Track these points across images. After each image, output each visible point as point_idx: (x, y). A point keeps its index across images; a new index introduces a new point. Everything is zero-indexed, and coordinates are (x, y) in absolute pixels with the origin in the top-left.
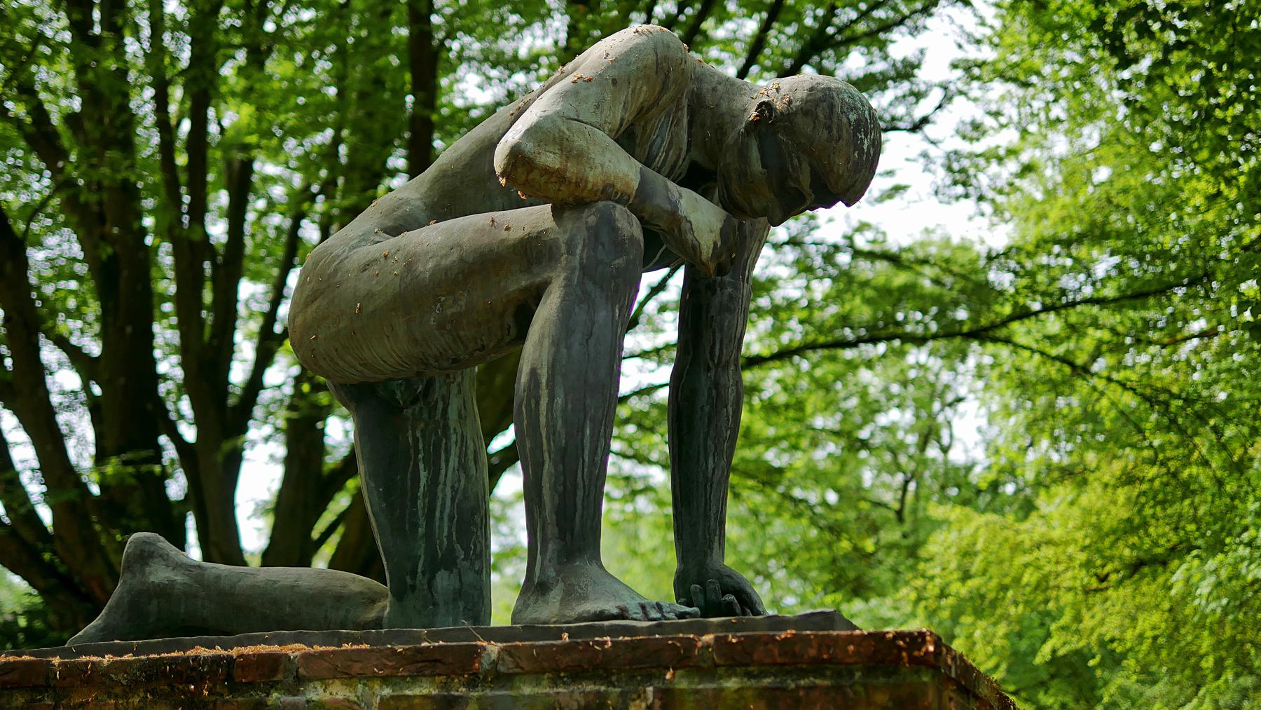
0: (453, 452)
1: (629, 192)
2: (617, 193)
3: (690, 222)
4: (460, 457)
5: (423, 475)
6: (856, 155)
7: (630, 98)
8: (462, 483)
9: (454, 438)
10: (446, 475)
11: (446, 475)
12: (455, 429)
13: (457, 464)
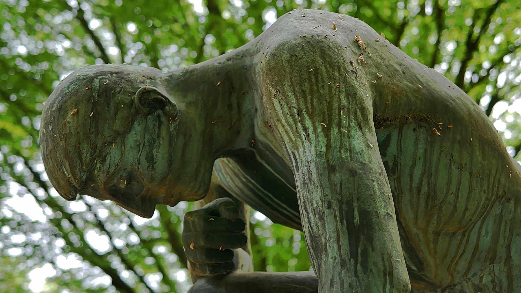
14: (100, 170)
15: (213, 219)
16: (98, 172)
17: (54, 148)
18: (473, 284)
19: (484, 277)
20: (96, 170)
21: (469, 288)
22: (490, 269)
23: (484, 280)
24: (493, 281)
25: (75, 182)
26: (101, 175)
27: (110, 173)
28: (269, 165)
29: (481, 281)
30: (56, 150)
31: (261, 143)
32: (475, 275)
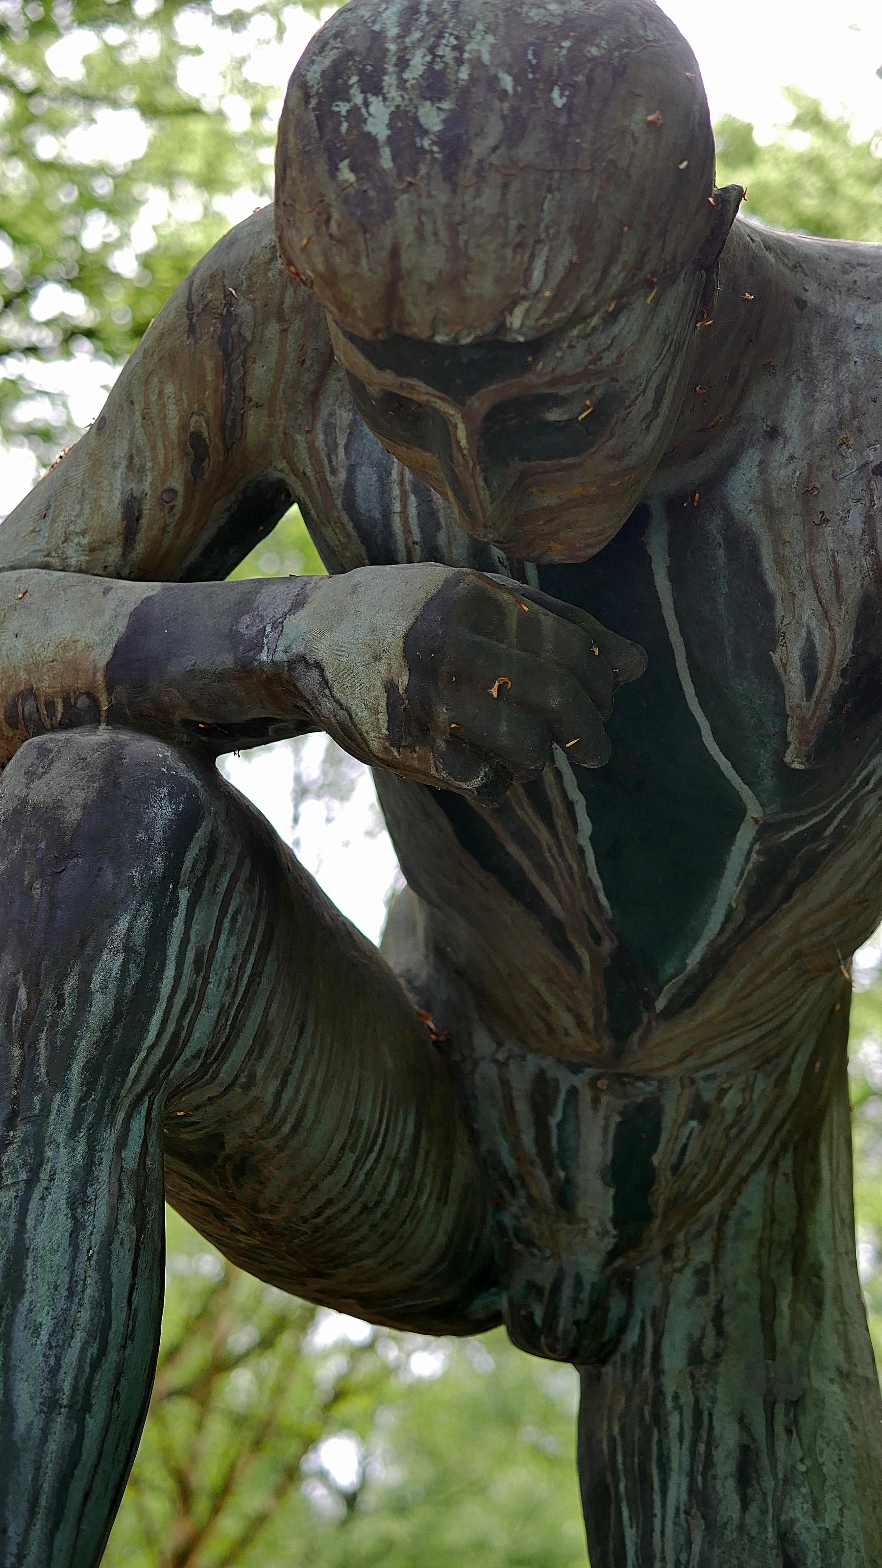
0: (675, 1464)
1: (81, 684)
2: (50, 705)
3: (318, 665)
4: (691, 1474)
5: (630, 1534)
6: (346, 174)
7: (141, 439)
8: (696, 1548)
9: (674, 1420)
10: (663, 1533)
11: (663, 1533)
12: (676, 1398)
13: (684, 1497)
14: (589, 335)
15: (597, 653)
16: (578, 337)
17: (551, 171)
18: (698, 1097)
19: (731, 1092)
20: (580, 327)
21: (678, 1102)
22: (747, 1080)
23: (727, 1099)
24: (740, 1110)
25: (537, 320)
26: (580, 351)
27: (599, 363)
28: (676, 576)
29: (720, 1098)
30: (554, 185)
31: (729, 517)
32: (711, 1077)
